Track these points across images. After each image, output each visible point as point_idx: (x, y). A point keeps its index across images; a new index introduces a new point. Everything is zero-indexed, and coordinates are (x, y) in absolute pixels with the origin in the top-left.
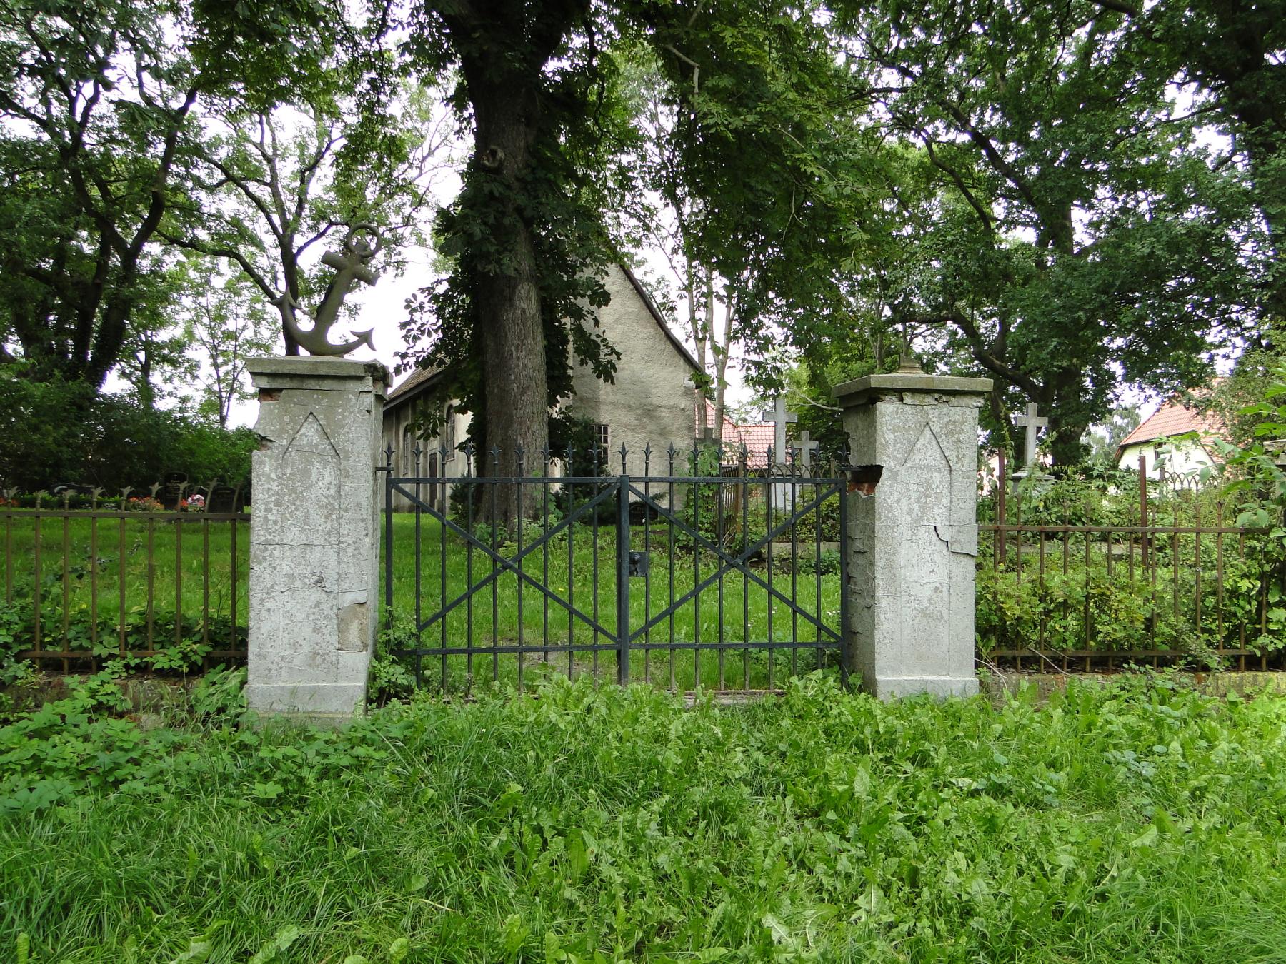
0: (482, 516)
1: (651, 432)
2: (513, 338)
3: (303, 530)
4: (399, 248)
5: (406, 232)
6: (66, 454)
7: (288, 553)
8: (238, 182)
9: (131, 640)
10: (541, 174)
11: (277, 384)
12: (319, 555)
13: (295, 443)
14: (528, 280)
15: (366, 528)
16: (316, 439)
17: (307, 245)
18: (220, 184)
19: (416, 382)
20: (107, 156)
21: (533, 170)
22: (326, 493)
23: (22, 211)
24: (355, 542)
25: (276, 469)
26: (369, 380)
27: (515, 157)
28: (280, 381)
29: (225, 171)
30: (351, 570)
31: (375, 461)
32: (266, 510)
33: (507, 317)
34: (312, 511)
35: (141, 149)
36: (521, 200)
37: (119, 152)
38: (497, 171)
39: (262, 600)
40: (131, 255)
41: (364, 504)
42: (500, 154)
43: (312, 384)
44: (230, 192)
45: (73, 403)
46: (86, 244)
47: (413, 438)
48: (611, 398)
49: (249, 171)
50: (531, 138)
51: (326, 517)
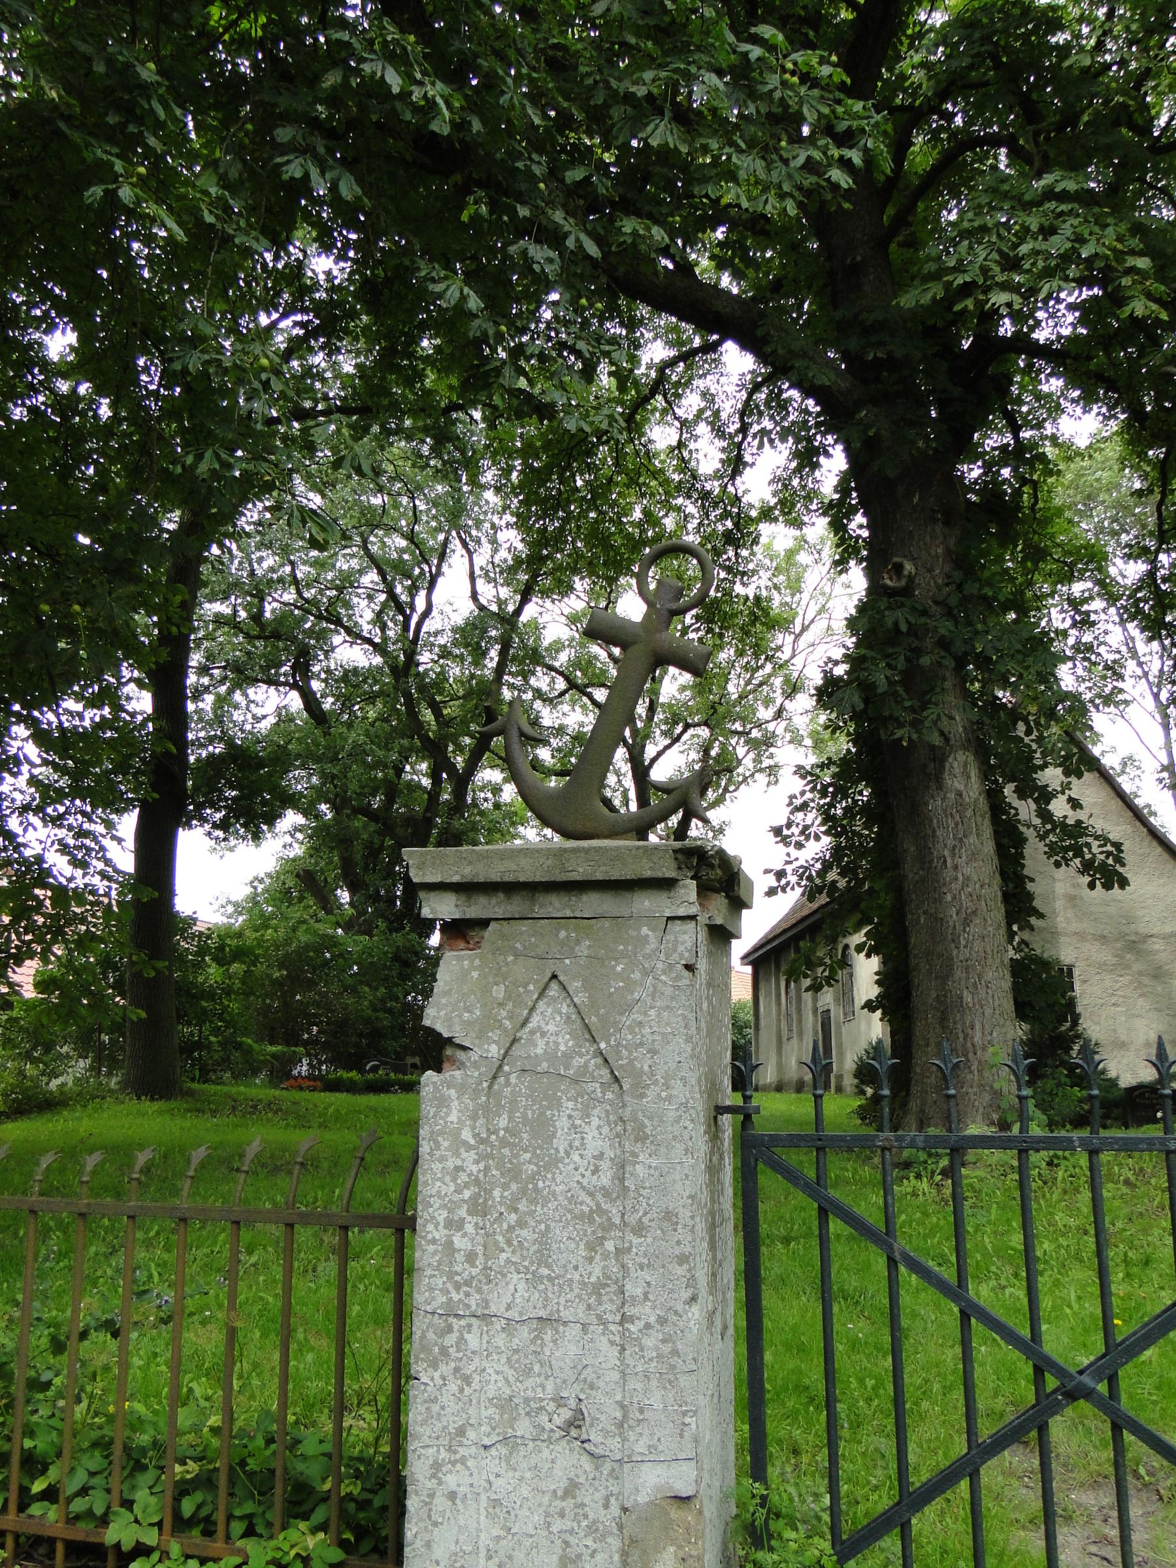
0: (911, 1120)
1: (1140, 973)
2: (945, 837)
3: (534, 1280)
4: (772, 750)
5: (779, 728)
6: (386, 1021)
7: (500, 1340)
8: (582, 690)
9: (188, 1507)
10: (971, 588)
11: (476, 909)
12: (573, 1350)
13: (517, 1051)
14: (965, 749)
15: (691, 1282)
16: (565, 1042)
17: (660, 754)
18: (562, 694)
19: (799, 916)
20: (442, 676)
21: (959, 587)
22: (589, 1180)
23: (346, 740)
24: (662, 1321)
25: (474, 1118)
26: (689, 889)
27: (930, 570)
28: (482, 900)
29: (567, 679)
30: (655, 1400)
31: (712, 1088)
32: (449, 1224)
33: (935, 805)
34: (557, 1231)
35: (476, 663)
36: (945, 627)
37: (454, 671)
38: (907, 591)
39: (437, 1466)
40: (462, 781)
41: (685, 1215)
42: (909, 567)
43: (555, 905)
44: (573, 703)
45: (396, 958)
46: (419, 772)
47: (798, 990)
48: (1075, 926)
49: (594, 674)
50: (952, 542)
51: (591, 1247)
